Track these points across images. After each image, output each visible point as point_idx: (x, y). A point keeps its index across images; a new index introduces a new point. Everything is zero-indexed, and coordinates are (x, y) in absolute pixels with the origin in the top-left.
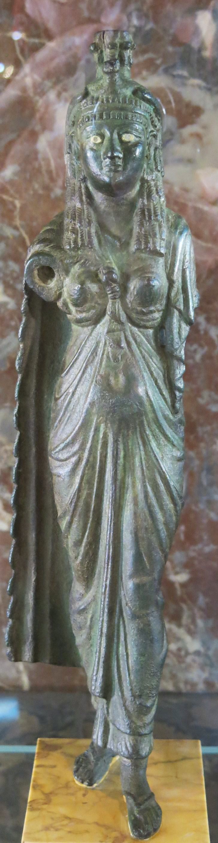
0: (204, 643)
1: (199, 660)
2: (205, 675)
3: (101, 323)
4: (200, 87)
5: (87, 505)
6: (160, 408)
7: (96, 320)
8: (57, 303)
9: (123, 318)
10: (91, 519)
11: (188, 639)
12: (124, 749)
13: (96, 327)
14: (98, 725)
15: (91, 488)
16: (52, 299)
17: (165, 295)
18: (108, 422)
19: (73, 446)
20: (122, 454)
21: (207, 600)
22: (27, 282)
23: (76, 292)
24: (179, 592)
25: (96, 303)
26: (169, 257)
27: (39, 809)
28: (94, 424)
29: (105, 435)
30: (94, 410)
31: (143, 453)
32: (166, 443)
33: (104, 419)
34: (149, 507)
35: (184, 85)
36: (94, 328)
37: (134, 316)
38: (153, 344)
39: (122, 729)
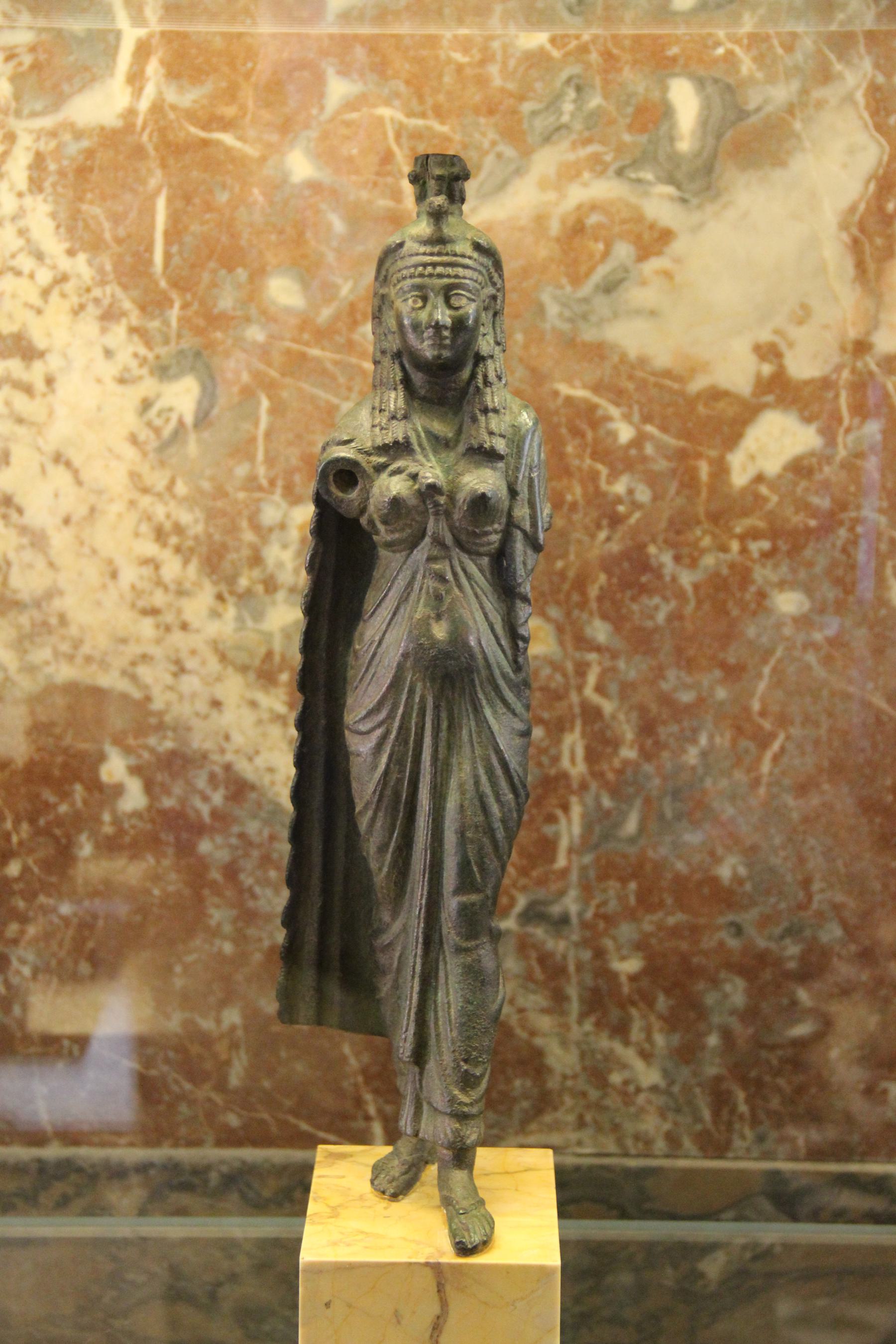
0: (665, 1073)
1: (660, 1100)
2: (667, 1126)
3: (419, 548)
4: (671, 198)
5: (397, 794)
6: (498, 663)
7: (413, 544)
8: (359, 520)
9: (449, 540)
10: (401, 815)
11: (639, 1065)
12: (442, 1136)
13: (412, 552)
14: (407, 1106)
15: (402, 771)
16: (353, 514)
17: (506, 509)
18: (427, 680)
19: (378, 713)
20: (444, 725)
21: (671, 1002)
22: (320, 491)
23: (386, 505)
24: (626, 989)
25: (413, 520)
26: (512, 461)
27: (322, 1223)
28: (408, 682)
29: (423, 698)
30: (408, 664)
31: (473, 723)
32: (505, 710)
33: (422, 676)
34: (481, 798)
35: (646, 194)
36: (408, 556)
37: (463, 537)
38: (488, 576)
39: (440, 1108)
